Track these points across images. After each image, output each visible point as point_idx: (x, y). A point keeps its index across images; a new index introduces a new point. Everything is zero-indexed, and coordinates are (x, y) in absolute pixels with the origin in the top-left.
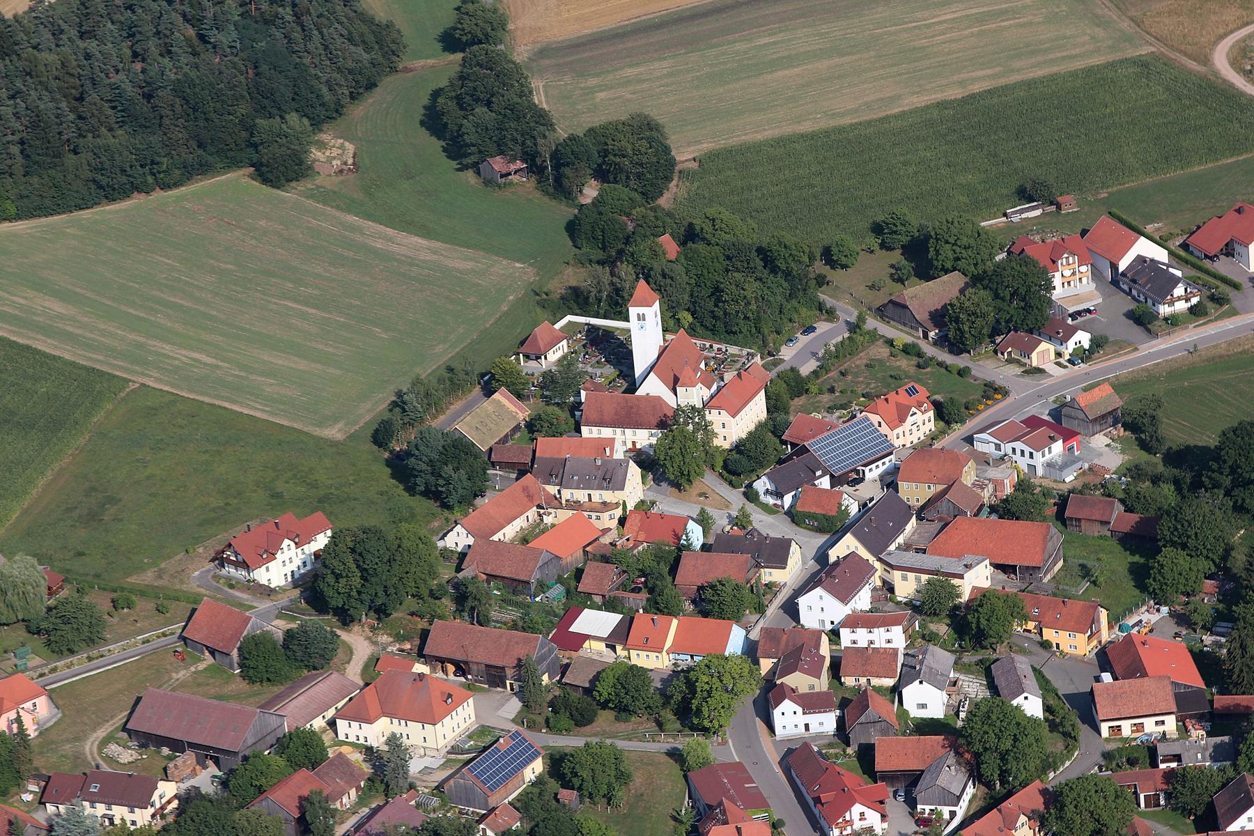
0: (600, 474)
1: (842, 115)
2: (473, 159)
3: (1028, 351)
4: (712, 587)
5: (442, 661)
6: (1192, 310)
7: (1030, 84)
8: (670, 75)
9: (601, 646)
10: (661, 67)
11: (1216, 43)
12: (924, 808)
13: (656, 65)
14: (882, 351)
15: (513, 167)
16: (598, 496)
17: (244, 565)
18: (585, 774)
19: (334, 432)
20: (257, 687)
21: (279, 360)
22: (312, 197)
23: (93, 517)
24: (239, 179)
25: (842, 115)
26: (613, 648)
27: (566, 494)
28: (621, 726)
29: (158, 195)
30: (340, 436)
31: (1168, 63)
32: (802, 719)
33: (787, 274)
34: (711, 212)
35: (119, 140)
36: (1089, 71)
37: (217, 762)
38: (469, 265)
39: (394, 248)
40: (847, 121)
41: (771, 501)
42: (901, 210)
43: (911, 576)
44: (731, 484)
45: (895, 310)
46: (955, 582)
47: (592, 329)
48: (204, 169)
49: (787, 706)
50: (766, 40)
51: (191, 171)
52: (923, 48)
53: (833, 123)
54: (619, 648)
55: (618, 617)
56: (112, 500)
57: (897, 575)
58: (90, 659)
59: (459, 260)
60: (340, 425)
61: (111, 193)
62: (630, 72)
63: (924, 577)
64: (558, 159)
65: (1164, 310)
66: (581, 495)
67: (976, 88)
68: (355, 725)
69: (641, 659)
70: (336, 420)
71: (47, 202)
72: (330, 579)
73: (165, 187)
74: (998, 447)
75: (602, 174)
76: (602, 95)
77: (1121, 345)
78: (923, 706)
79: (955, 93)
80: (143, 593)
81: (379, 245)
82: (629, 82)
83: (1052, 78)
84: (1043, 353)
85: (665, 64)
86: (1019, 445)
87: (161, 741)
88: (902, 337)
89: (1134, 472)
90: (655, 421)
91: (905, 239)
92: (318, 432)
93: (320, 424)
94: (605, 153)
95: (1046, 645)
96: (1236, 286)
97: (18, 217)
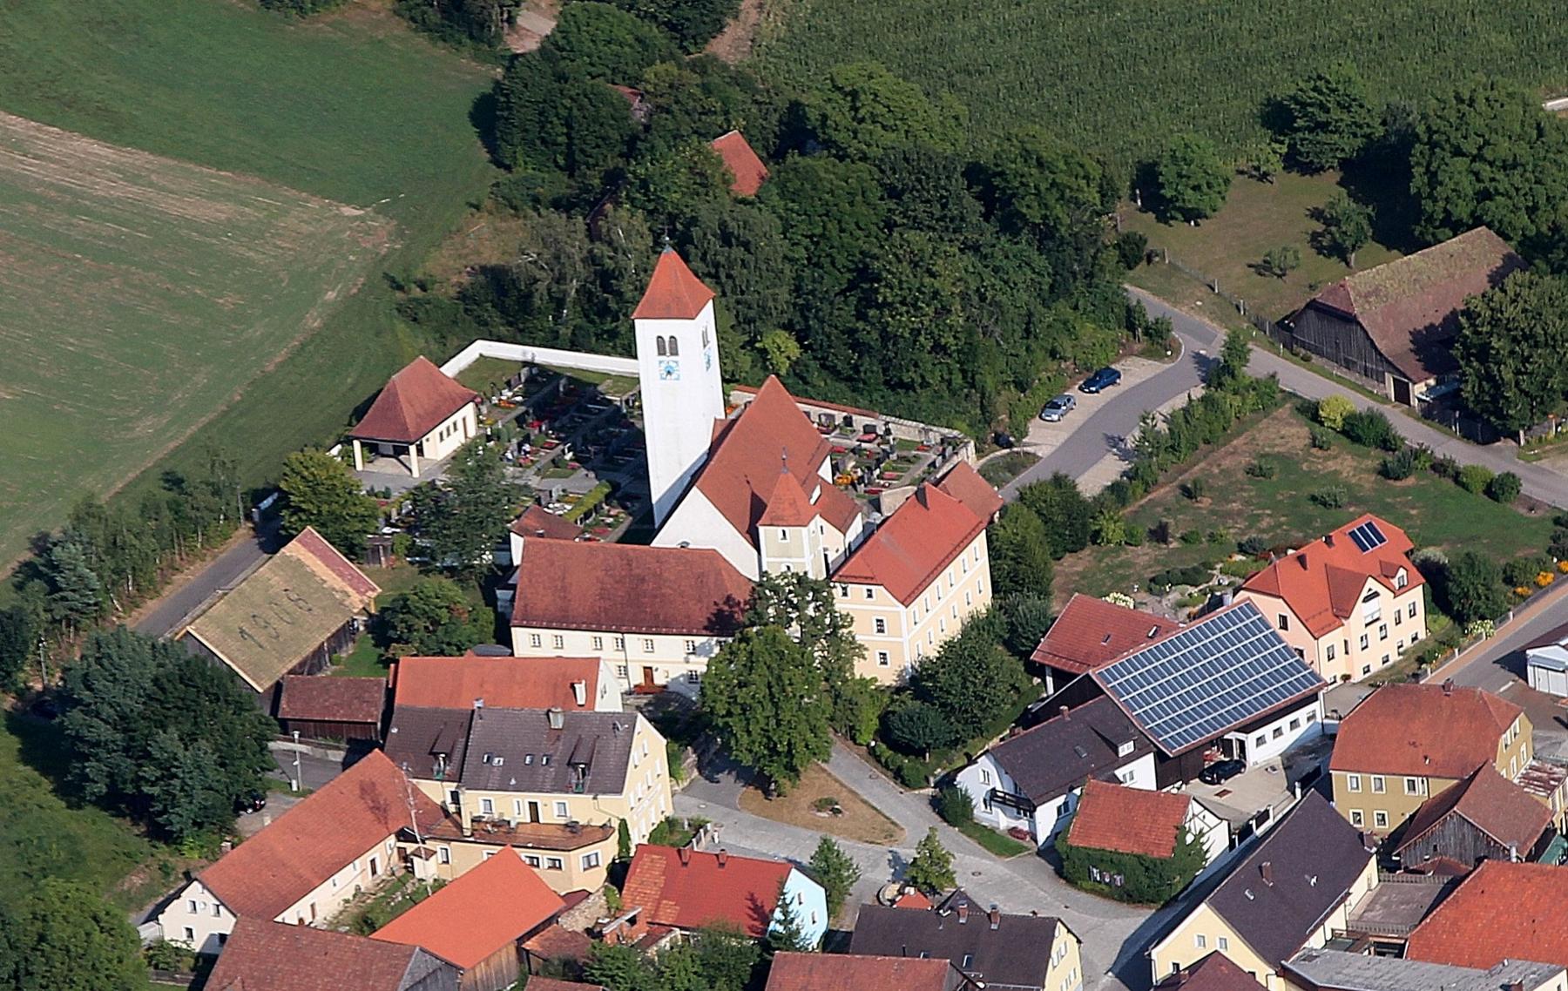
0: (561, 751)
14: (1292, 435)
16: (555, 807)
27: (474, 803)
34: (848, 73)
38: (222, 211)
39: (31, 168)
41: (1002, 820)
42: (1339, 68)
44: (899, 776)
47: (540, 376)
66: (511, 806)
90: (702, 615)
91: (1350, 145)
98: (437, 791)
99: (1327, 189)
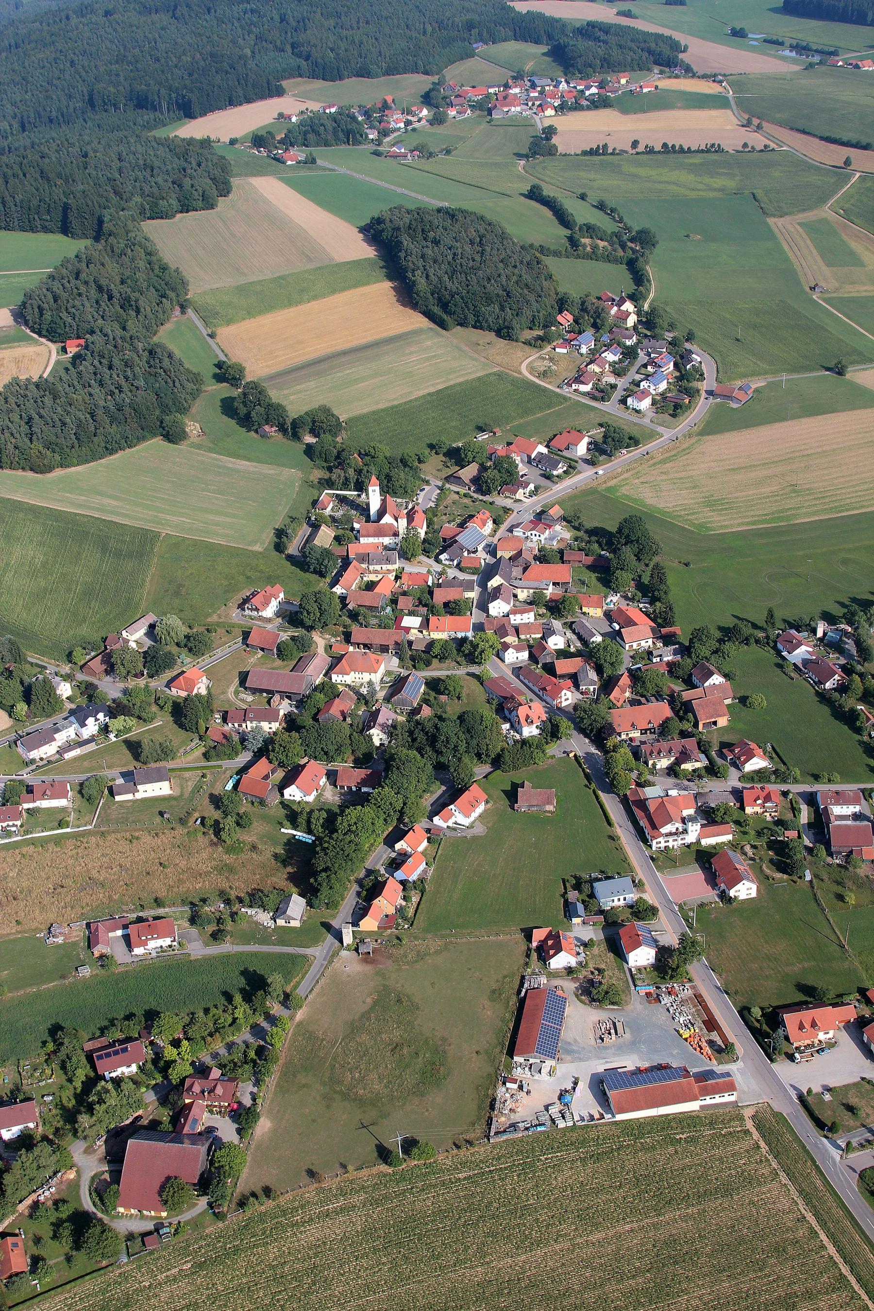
0: (385, 558)
1: (393, 400)
2: (255, 428)
3: (515, 493)
4: (455, 602)
5: (358, 644)
6: (564, 472)
7: (460, 384)
8: (317, 387)
9: (416, 631)
10: (312, 384)
11: (521, 363)
12: (583, 688)
13: (309, 384)
14: (456, 497)
15: (273, 429)
16: (385, 567)
17: (257, 610)
18: (451, 689)
19: (258, 548)
20: (285, 662)
21: (218, 519)
22: (191, 447)
23: (177, 593)
24: (157, 441)
25: (393, 400)
26: (421, 632)
27: (371, 568)
28: (443, 665)
29: (128, 450)
30: (261, 550)
31: (507, 374)
32: (516, 655)
33: (411, 468)
34: (372, 444)
35: (113, 429)
36: (479, 378)
37: (289, 698)
38: (272, 472)
39: (238, 467)
40: (396, 403)
41: (447, 563)
42: (443, 438)
43: (525, 590)
44: (428, 557)
45: (457, 480)
46: (545, 591)
47: (337, 496)
48: (144, 438)
49: (511, 650)
50: (348, 372)
51: (141, 439)
52: (411, 372)
53: (390, 404)
54: (424, 632)
55: (420, 619)
56: (181, 585)
57: (519, 590)
58: (210, 657)
59: (268, 470)
60: (259, 544)
61: (112, 452)
62: (299, 387)
63: (531, 591)
64: (295, 424)
65: (555, 473)
66: (378, 567)
67: (440, 387)
68: (340, 676)
69: (436, 635)
70: (256, 543)
71: (89, 457)
72: (305, 614)
73: (130, 447)
74: (524, 533)
75: (314, 432)
76: (292, 397)
77: (546, 489)
78: (556, 644)
79: (432, 390)
80: (218, 624)
81: (231, 465)
82: (300, 392)
83: (467, 382)
84: (520, 494)
85: (312, 383)
86: (534, 532)
87: (262, 691)
88: (463, 491)
89: (576, 539)
90: (391, 533)
91: (445, 450)
92: (250, 548)
93: (250, 544)
94: (314, 422)
95: (584, 614)
96: (576, 462)
97: (78, 465)
98: (364, 566)
99: (441, 457)
